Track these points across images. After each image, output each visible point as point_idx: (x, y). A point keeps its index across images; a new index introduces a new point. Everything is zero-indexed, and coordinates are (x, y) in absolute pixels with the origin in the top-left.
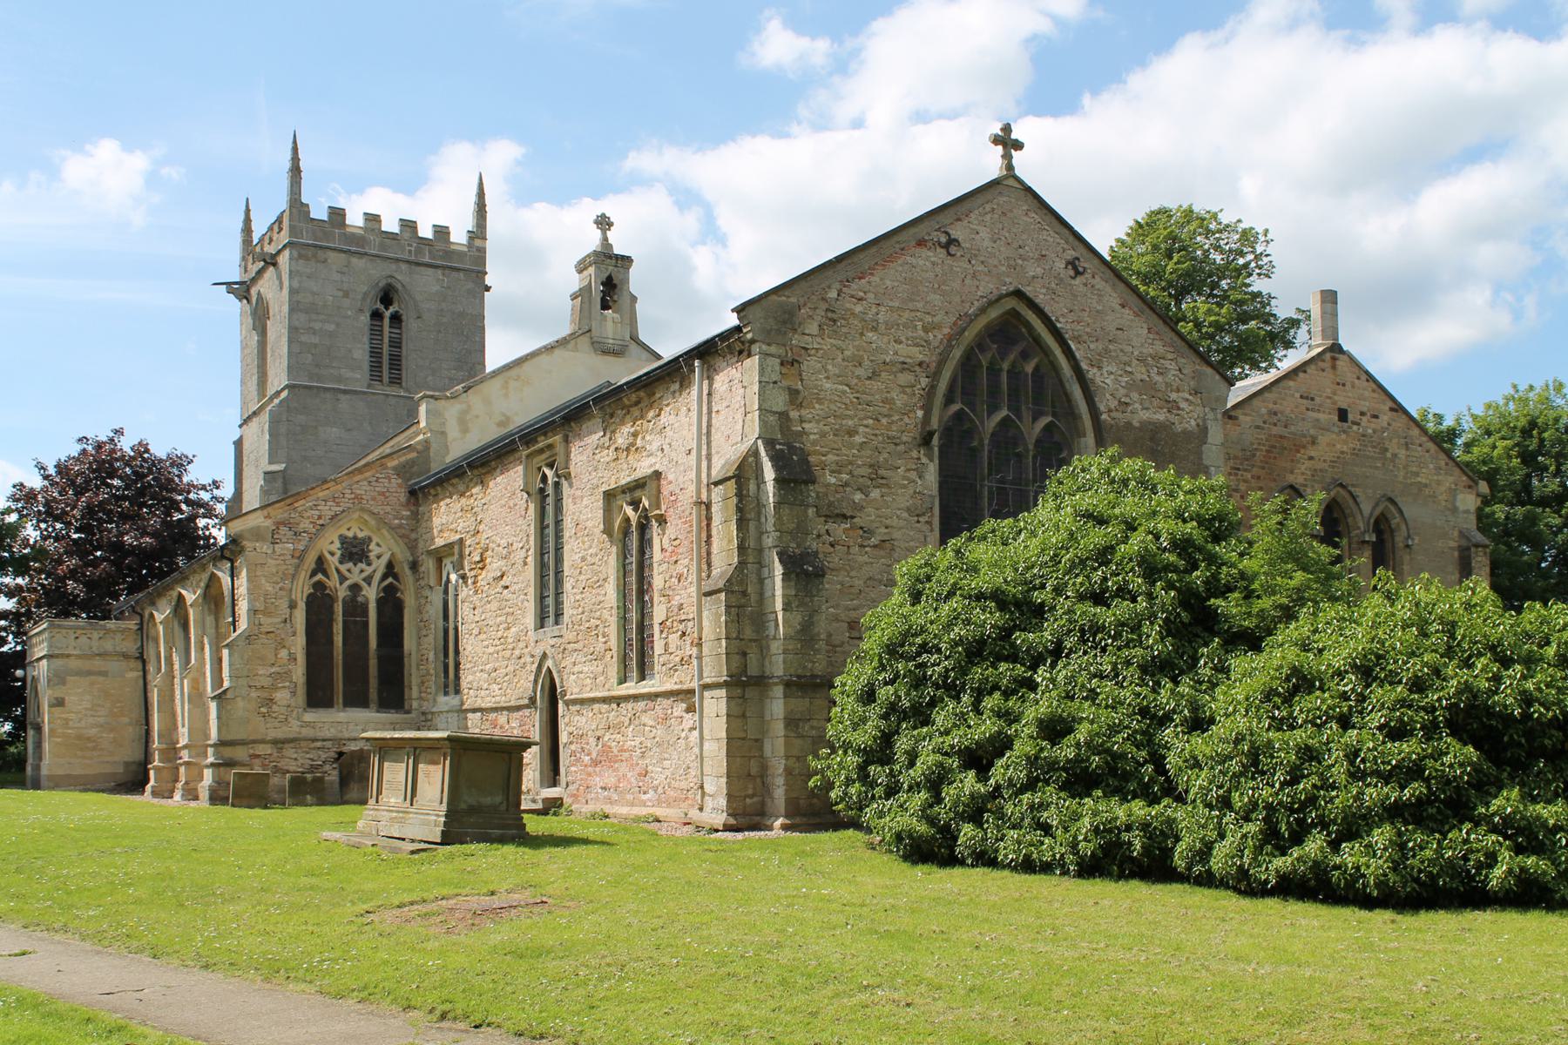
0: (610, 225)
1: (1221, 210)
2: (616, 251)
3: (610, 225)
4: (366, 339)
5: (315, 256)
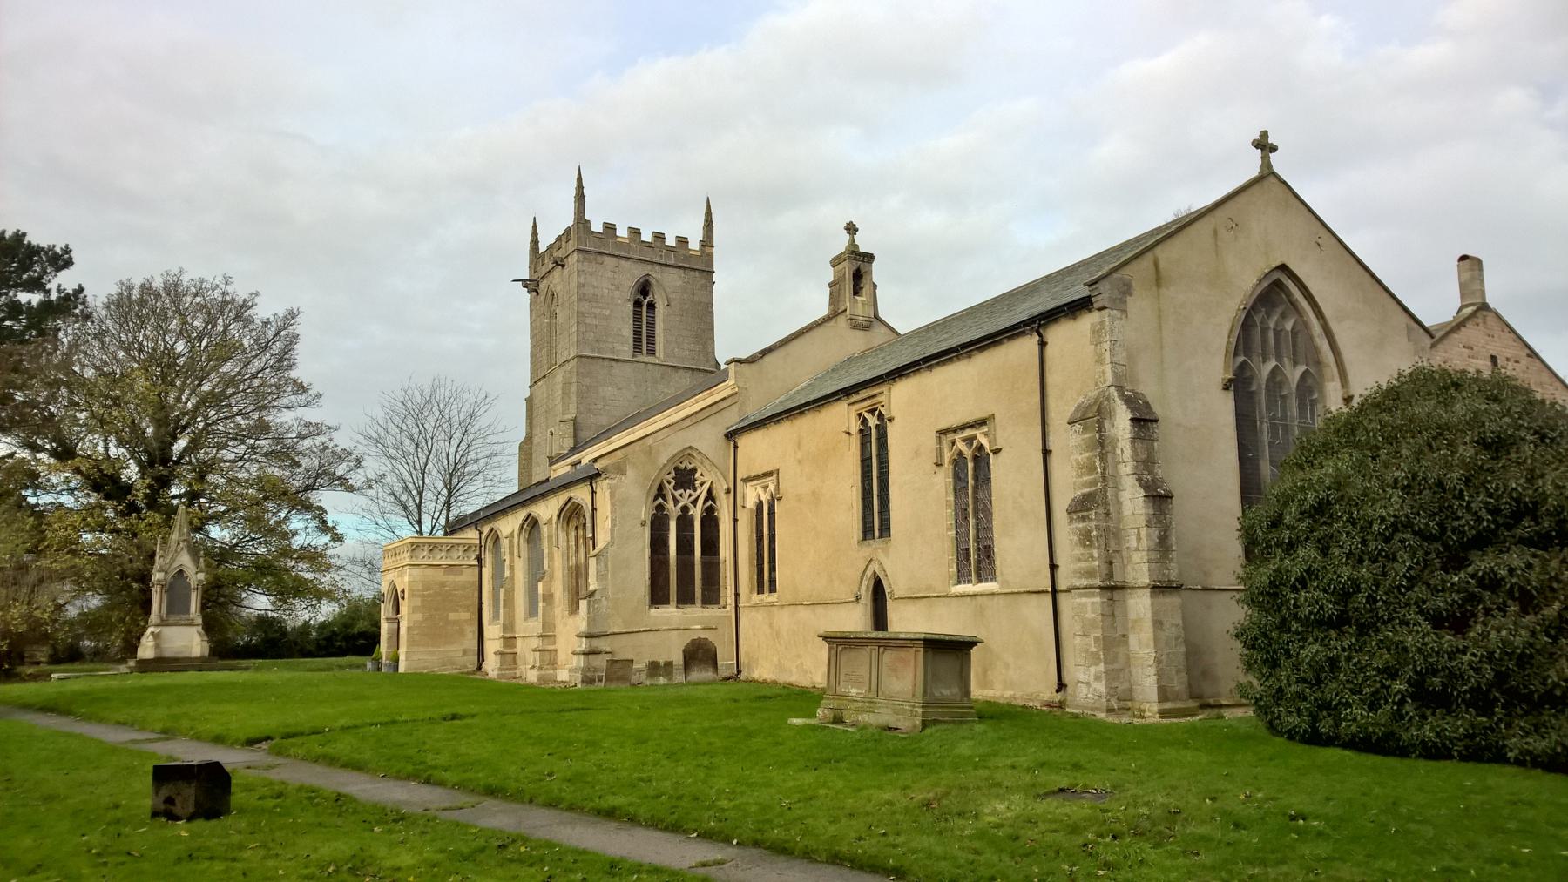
0: (856, 230)
1: (851, 229)
2: (862, 249)
3: (856, 230)
4: (631, 322)
5: (595, 259)
